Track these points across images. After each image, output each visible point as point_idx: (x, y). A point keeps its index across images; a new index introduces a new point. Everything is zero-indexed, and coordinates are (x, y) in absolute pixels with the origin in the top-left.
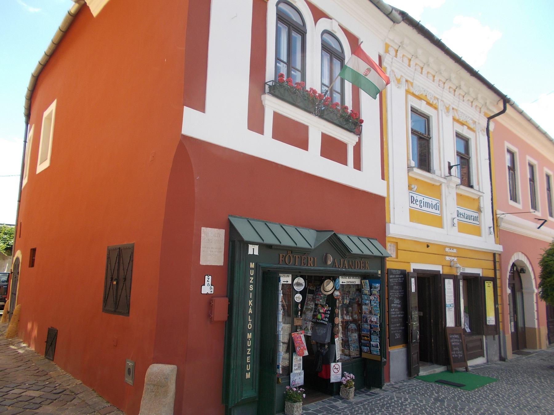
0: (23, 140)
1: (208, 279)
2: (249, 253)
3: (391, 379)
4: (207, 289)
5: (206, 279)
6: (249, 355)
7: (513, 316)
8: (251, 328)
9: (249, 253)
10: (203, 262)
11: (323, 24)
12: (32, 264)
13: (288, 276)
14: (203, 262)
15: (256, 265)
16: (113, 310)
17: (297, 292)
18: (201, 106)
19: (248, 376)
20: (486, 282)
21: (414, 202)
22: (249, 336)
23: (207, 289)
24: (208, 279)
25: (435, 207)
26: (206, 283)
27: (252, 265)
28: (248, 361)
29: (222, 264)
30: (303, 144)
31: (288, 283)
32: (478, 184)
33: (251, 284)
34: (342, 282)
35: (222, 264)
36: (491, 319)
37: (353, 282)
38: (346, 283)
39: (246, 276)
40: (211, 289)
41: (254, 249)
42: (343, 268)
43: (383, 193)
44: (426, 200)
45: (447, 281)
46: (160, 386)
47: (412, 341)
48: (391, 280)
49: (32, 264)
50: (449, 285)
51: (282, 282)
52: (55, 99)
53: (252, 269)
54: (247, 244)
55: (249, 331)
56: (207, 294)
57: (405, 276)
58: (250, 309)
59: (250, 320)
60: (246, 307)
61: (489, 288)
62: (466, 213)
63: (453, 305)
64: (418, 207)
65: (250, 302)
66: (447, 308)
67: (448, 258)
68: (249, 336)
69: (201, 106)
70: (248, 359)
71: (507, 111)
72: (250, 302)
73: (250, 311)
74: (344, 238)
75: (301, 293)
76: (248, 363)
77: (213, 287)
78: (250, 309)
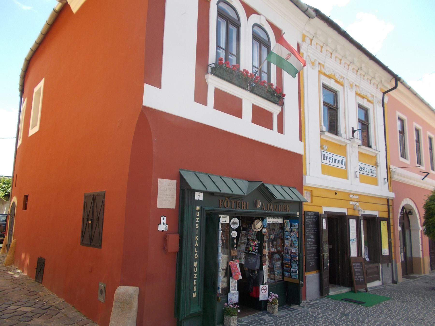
0: (18, 110)
1: (164, 220)
2: (196, 199)
3: (307, 298)
4: (163, 227)
5: (162, 219)
6: (195, 279)
7: (403, 248)
8: (197, 258)
9: (196, 199)
10: (159, 206)
11: (254, 19)
12: (25, 207)
13: (226, 217)
14: (159, 206)
15: (201, 208)
16: (89, 243)
17: (233, 230)
18: (158, 84)
19: (195, 295)
20: (381, 221)
21: (325, 159)
22: (196, 264)
23: (163, 227)
24: (164, 220)
25: (342, 162)
26: (162, 222)
27: (198, 208)
28: (195, 284)
29: (174, 208)
30: (238, 113)
31: (226, 222)
32: (376, 144)
33: (197, 223)
34: (269, 222)
35: (174, 208)
36: (385, 251)
37: (277, 222)
38: (271, 223)
39: (193, 217)
40: (166, 227)
41: (199, 195)
42: (269, 210)
43: (301, 152)
44: (335, 157)
45: (351, 221)
46: (125, 303)
47: (323, 268)
48: (307, 220)
49: (25, 207)
50: (353, 224)
51: (221, 222)
52: (43, 78)
53: (198, 211)
54: (194, 191)
55: (196, 260)
56: (163, 231)
57: (318, 217)
58: (197, 243)
59: (196, 252)
60: (193, 241)
61: (384, 226)
62: (366, 168)
63: (356, 240)
64: (328, 162)
65: (197, 238)
66: (351, 242)
67: (351, 203)
68: (196, 264)
69: (158, 84)
70: (195, 282)
71: (398, 87)
72: (197, 238)
73: (197, 244)
74: (270, 187)
75: (236, 230)
76: (195, 285)
77: (167, 225)
78: (197, 243)
